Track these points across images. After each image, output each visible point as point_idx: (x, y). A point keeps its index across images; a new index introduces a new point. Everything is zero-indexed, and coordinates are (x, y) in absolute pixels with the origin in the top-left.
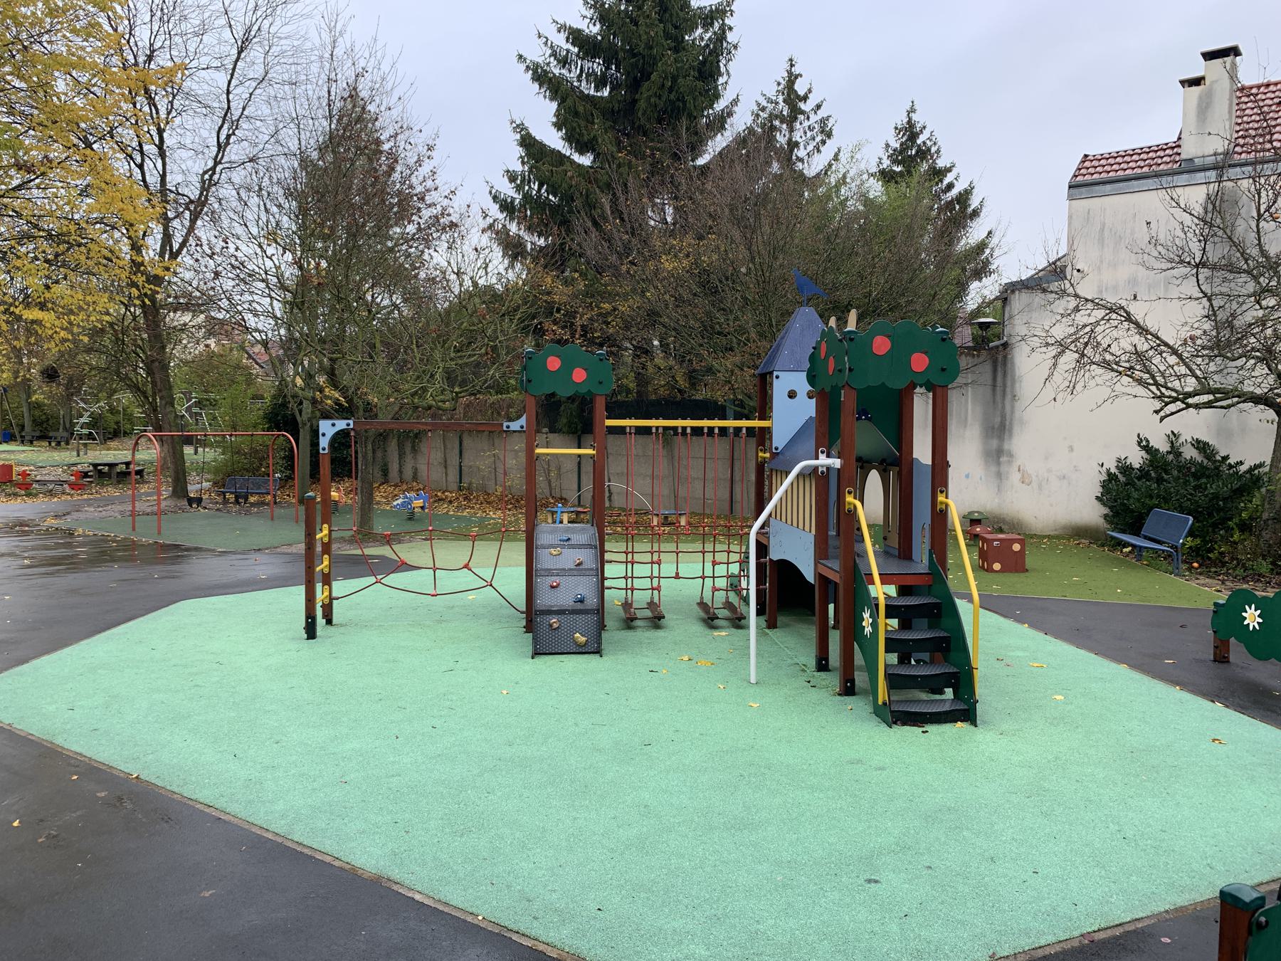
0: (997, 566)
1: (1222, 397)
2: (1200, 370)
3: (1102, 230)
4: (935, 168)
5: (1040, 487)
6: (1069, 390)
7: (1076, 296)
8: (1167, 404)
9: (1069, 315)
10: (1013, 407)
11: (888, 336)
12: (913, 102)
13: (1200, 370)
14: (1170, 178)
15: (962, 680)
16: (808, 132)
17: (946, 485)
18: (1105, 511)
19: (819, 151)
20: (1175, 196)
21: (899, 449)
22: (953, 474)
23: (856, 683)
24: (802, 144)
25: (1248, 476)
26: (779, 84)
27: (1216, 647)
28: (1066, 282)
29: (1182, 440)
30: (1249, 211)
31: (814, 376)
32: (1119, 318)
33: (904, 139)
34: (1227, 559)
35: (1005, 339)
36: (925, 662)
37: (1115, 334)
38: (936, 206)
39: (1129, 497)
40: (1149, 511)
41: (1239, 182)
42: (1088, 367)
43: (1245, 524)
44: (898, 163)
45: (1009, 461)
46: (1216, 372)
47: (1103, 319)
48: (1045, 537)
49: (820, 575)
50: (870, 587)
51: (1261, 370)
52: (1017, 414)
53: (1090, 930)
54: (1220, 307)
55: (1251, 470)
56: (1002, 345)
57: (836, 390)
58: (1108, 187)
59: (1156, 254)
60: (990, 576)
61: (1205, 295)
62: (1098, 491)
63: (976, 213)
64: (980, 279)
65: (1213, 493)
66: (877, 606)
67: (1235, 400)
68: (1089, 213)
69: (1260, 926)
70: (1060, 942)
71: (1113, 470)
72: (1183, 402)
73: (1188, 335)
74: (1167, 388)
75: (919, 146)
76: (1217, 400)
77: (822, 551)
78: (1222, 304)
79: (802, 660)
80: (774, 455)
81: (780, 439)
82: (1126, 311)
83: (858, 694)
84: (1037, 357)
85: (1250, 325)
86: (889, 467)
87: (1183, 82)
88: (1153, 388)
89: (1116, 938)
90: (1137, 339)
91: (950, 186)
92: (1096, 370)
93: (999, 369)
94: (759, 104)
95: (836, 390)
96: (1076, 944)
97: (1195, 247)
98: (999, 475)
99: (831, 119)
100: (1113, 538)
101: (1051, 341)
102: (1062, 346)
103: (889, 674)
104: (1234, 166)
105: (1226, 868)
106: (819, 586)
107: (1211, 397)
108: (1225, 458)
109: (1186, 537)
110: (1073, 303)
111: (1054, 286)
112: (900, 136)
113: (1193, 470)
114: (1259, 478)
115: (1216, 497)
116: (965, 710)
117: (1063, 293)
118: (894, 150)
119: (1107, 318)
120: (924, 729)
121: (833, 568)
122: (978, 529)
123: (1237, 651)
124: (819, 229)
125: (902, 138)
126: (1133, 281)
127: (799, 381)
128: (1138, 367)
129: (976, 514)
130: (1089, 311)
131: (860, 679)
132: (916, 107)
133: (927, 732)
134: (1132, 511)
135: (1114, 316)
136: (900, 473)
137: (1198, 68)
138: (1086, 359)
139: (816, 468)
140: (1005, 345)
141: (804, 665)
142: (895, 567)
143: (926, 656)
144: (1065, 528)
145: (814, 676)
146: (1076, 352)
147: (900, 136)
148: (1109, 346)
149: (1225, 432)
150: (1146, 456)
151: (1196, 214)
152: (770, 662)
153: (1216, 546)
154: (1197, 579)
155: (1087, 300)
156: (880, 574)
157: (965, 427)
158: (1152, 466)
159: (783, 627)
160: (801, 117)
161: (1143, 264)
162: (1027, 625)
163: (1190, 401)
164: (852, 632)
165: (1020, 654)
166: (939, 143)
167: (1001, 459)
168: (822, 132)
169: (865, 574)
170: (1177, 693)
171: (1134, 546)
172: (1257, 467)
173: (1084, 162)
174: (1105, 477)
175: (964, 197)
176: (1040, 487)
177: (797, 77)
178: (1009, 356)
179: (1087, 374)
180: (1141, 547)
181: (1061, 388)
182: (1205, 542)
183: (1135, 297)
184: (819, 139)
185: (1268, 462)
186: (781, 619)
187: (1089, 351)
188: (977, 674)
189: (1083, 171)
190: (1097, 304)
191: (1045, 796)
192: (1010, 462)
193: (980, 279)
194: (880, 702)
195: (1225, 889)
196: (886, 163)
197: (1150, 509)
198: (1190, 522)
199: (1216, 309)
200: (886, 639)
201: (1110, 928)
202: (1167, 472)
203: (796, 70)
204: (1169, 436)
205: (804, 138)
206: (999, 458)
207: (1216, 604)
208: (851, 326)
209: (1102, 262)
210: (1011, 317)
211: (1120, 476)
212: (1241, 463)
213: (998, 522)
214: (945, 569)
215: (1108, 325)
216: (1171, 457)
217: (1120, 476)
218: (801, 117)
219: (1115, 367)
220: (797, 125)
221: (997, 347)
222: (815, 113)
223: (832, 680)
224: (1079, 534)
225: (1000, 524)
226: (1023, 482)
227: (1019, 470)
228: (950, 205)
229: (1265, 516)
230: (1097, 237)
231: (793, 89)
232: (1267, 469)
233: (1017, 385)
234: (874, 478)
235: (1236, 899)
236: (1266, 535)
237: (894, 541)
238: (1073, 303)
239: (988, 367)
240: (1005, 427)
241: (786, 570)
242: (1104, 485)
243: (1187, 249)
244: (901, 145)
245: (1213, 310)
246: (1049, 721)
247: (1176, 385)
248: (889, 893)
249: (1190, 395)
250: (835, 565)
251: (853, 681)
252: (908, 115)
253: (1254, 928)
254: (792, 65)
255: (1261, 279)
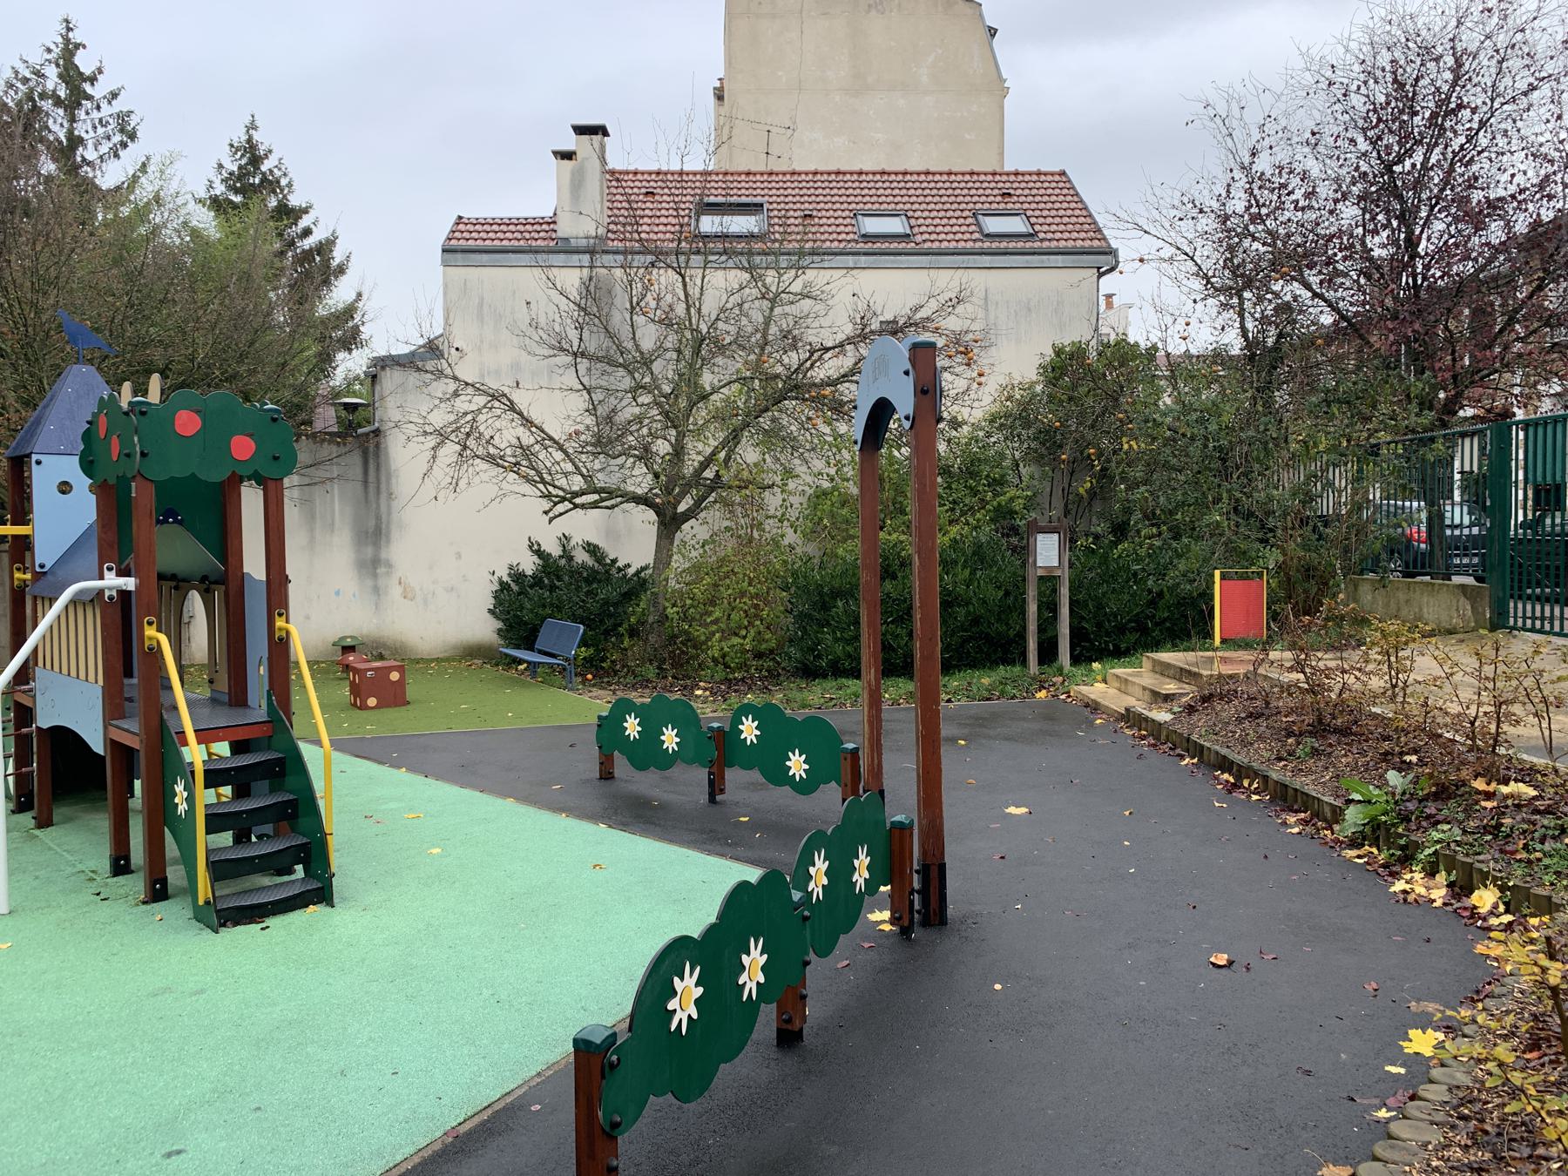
0: (372, 702)
1: (609, 497)
2: (585, 467)
3: (481, 305)
4: (286, 205)
5: (425, 602)
6: (451, 487)
7: (455, 378)
8: (556, 504)
9: (448, 399)
10: (389, 507)
11: (197, 412)
12: (253, 116)
13: (585, 467)
14: (545, 256)
15: (313, 853)
16: (99, 126)
17: (286, 607)
18: (499, 625)
19: (117, 156)
20: (551, 276)
21: (224, 561)
22: (294, 591)
23: (169, 881)
24: (90, 142)
25: (635, 578)
26: (49, 51)
27: (601, 764)
28: (443, 361)
29: (573, 543)
30: (624, 303)
31: (92, 462)
32: (502, 406)
33: (243, 162)
34: (618, 667)
35: (377, 425)
36: (268, 836)
37: (498, 424)
38: (290, 254)
39: (522, 608)
40: (543, 622)
41: (613, 270)
42: (471, 461)
43: (633, 630)
44: (237, 191)
45: (388, 573)
46: (599, 470)
47: (485, 407)
48: (432, 660)
49: (113, 742)
50: (184, 750)
51: (641, 469)
52: (395, 516)
53: (455, 1124)
54: (600, 402)
55: (638, 573)
56: (373, 432)
57: (124, 482)
58: (485, 257)
59: (538, 339)
60: (364, 714)
61: (585, 388)
62: (490, 602)
63: (341, 270)
64: (350, 350)
65: (602, 599)
66: (193, 773)
67: (619, 499)
68: (465, 284)
69: (612, 1066)
70: (420, 1150)
71: (506, 579)
72: (571, 502)
73: (572, 429)
74: (555, 487)
75: (264, 174)
76: (603, 500)
77: (114, 706)
78: (601, 398)
79: (92, 864)
80: (38, 576)
81: (46, 553)
82: (509, 400)
83: (174, 896)
84: (413, 447)
85: (629, 422)
86: (213, 586)
87: (555, 153)
88: (541, 486)
89: (483, 1123)
90: (521, 431)
91: (307, 232)
92: (481, 465)
93: (371, 461)
94: (17, 73)
95: (124, 482)
96: (438, 1146)
97: (573, 335)
98: (376, 590)
99: (133, 116)
100: (506, 655)
101: (429, 429)
102: (442, 435)
103: (212, 862)
104: (607, 252)
105: (600, 1006)
106: (112, 758)
107: (596, 497)
108: (614, 561)
109: (579, 647)
110: (452, 386)
111: (430, 365)
112: (238, 156)
113: (585, 574)
114: (645, 581)
115: (606, 602)
116: (318, 889)
117: (439, 374)
118: (230, 174)
119: (489, 405)
120: (263, 925)
121: (131, 732)
122: (351, 658)
123: (621, 766)
124: (117, 262)
125: (240, 159)
126: (516, 366)
127: (70, 468)
128: (524, 463)
129: (349, 640)
130: (469, 397)
131: (175, 875)
132: (258, 123)
133: (268, 927)
134: (526, 623)
135: (497, 404)
136: (226, 594)
137: (570, 142)
138: (469, 452)
139: (101, 592)
140: (377, 432)
141: (93, 872)
142: (223, 719)
143: (268, 829)
144: (455, 647)
145: (107, 884)
146: (458, 443)
147: (238, 156)
148: (492, 437)
149: (611, 533)
150: (538, 561)
151: (572, 299)
152: (37, 878)
153: (608, 655)
154: (590, 691)
155: (467, 384)
156: (195, 731)
157: (333, 531)
158: (544, 572)
159: (64, 823)
160: (87, 104)
161: (525, 348)
162: (404, 769)
163: (578, 501)
164: (160, 813)
165: (393, 805)
166: (290, 175)
167: (378, 571)
168: (122, 131)
169: (176, 733)
170: (563, 822)
171: (529, 663)
172: (643, 569)
173: (458, 224)
174: (496, 587)
175: (325, 248)
176: (425, 602)
177: (77, 46)
178: (382, 446)
179: (470, 469)
180: (535, 663)
181: (443, 485)
182: (598, 651)
183: (518, 384)
184: (117, 138)
185: (652, 562)
186: (58, 813)
187: (471, 443)
188: (332, 842)
189: (457, 235)
190: (478, 389)
191: (412, 975)
192: (388, 574)
193: (350, 350)
194: (201, 902)
195: (578, 1036)
196: (219, 189)
197: (543, 619)
198: (581, 631)
199: (596, 403)
200: (207, 816)
201: (477, 1113)
202: (559, 578)
203: (76, 37)
204: (560, 539)
205: (92, 134)
206: (375, 568)
207: (600, 718)
208: (154, 396)
209: (482, 342)
210: (382, 398)
211: (513, 585)
212: (628, 566)
213: (377, 648)
214: (289, 714)
215: (490, 415)
216: (563, 562)
217: (513, 585)
218: (87, 104)
219: (501, 462)
220: (81, 114)
221: (367, 434)
222: (110, 103)
223: (135, 884)
224: (474, 654)
225: (378, 650)
226: (405, 597)
227: (400, 583)
228: (308, 255)
229: (651, 619)
230: (476, 312)
231: (73, 63)
232: (651, 571)
233: (394, 481)
234: (195, 603)
235: (587, 1043)
236: (652, 639)
237: (223, 684)
238: (452, 386)
239: (356, 459)
240: (380, 533)
241: (63, 740)
242: (496, 595)
243: (564, 335)
244: (240, 167)
245: (593, 404)
246: (422, 882)
247: (562, 482)
248: (197, 1163)
249: (577, 494)
250: (133, 725)
251: (164, 881)
252: (248, 131)
253: (607, 1069)
254: (69, 29)
255: (636, 375)
